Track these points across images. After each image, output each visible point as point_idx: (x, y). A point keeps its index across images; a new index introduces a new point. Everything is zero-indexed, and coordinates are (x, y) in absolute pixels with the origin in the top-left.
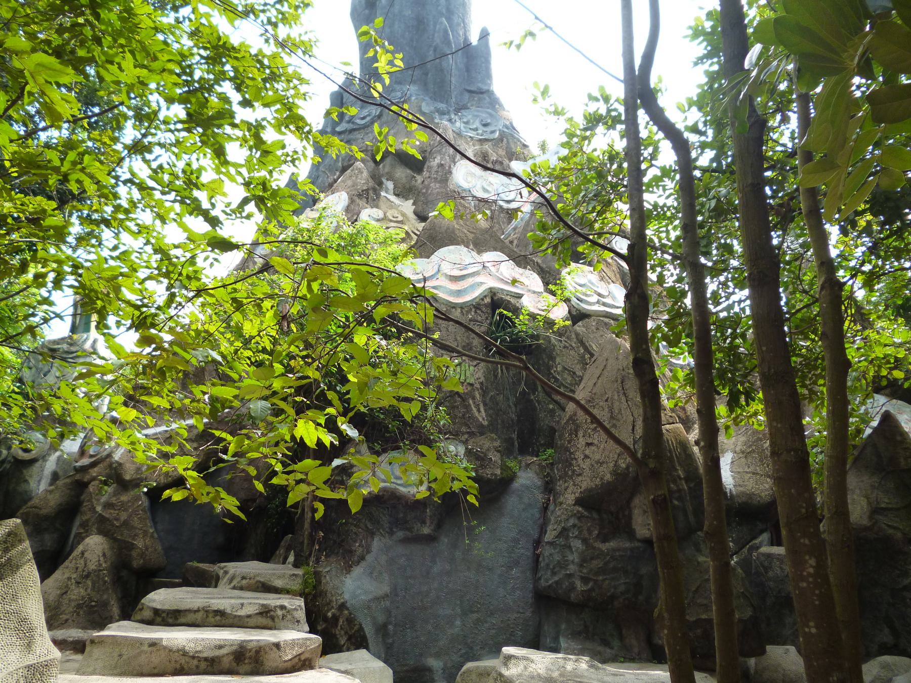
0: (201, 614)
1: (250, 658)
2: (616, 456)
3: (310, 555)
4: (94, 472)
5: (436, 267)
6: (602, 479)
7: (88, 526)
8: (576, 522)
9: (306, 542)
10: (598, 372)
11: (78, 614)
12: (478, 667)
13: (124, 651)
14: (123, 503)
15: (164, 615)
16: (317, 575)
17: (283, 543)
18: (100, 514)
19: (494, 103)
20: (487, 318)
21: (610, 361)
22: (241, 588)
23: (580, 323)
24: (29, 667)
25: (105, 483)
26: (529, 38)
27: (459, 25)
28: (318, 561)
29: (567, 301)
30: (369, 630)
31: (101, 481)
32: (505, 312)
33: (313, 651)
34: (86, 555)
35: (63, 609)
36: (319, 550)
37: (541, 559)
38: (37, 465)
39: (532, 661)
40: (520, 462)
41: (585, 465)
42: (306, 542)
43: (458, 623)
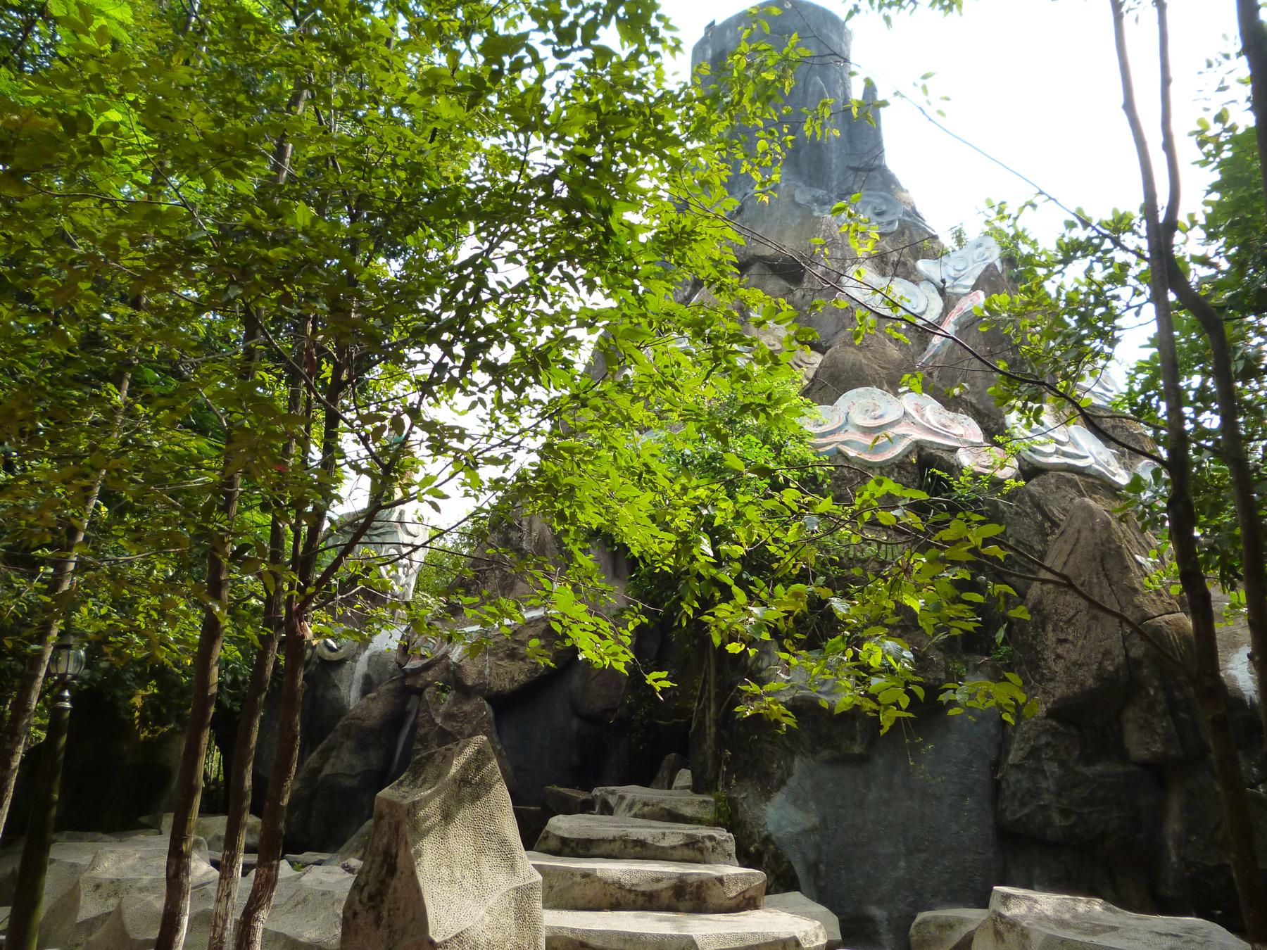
0: (618, 844)
1: (691, 893)
2: (1100, 656)
3: (717, 778)
4: (429, 676)
5: (843, 416)
6: (1082, 685)
8: (1050, 739)
9: (710, 762)
10: (1068, 548)
12: (936, 917)
13: (554, 882)
14: (466, 714)
15: (573, 845)
16: (732, 802)
17: (664, 764)
19: (888, 182)
20: (914, 481)
21: (1085, 533)
22: (644, 817)
23: (1034, 481)
24: (517, 889)
25: (443, 689)
26: (1028, 207)
27: (836, 81)
28: (727, 785)
29: (1017, 454)
30: (799, 869)
31: (438, 686)
32: (939, 472)
33: (757, 888)
36: (728, 772)
37: (1004, 785)
39: (1036, 902)
40: (966, 663)
41: (1058, 668)
42: (710, 762)
43: (902, 864)
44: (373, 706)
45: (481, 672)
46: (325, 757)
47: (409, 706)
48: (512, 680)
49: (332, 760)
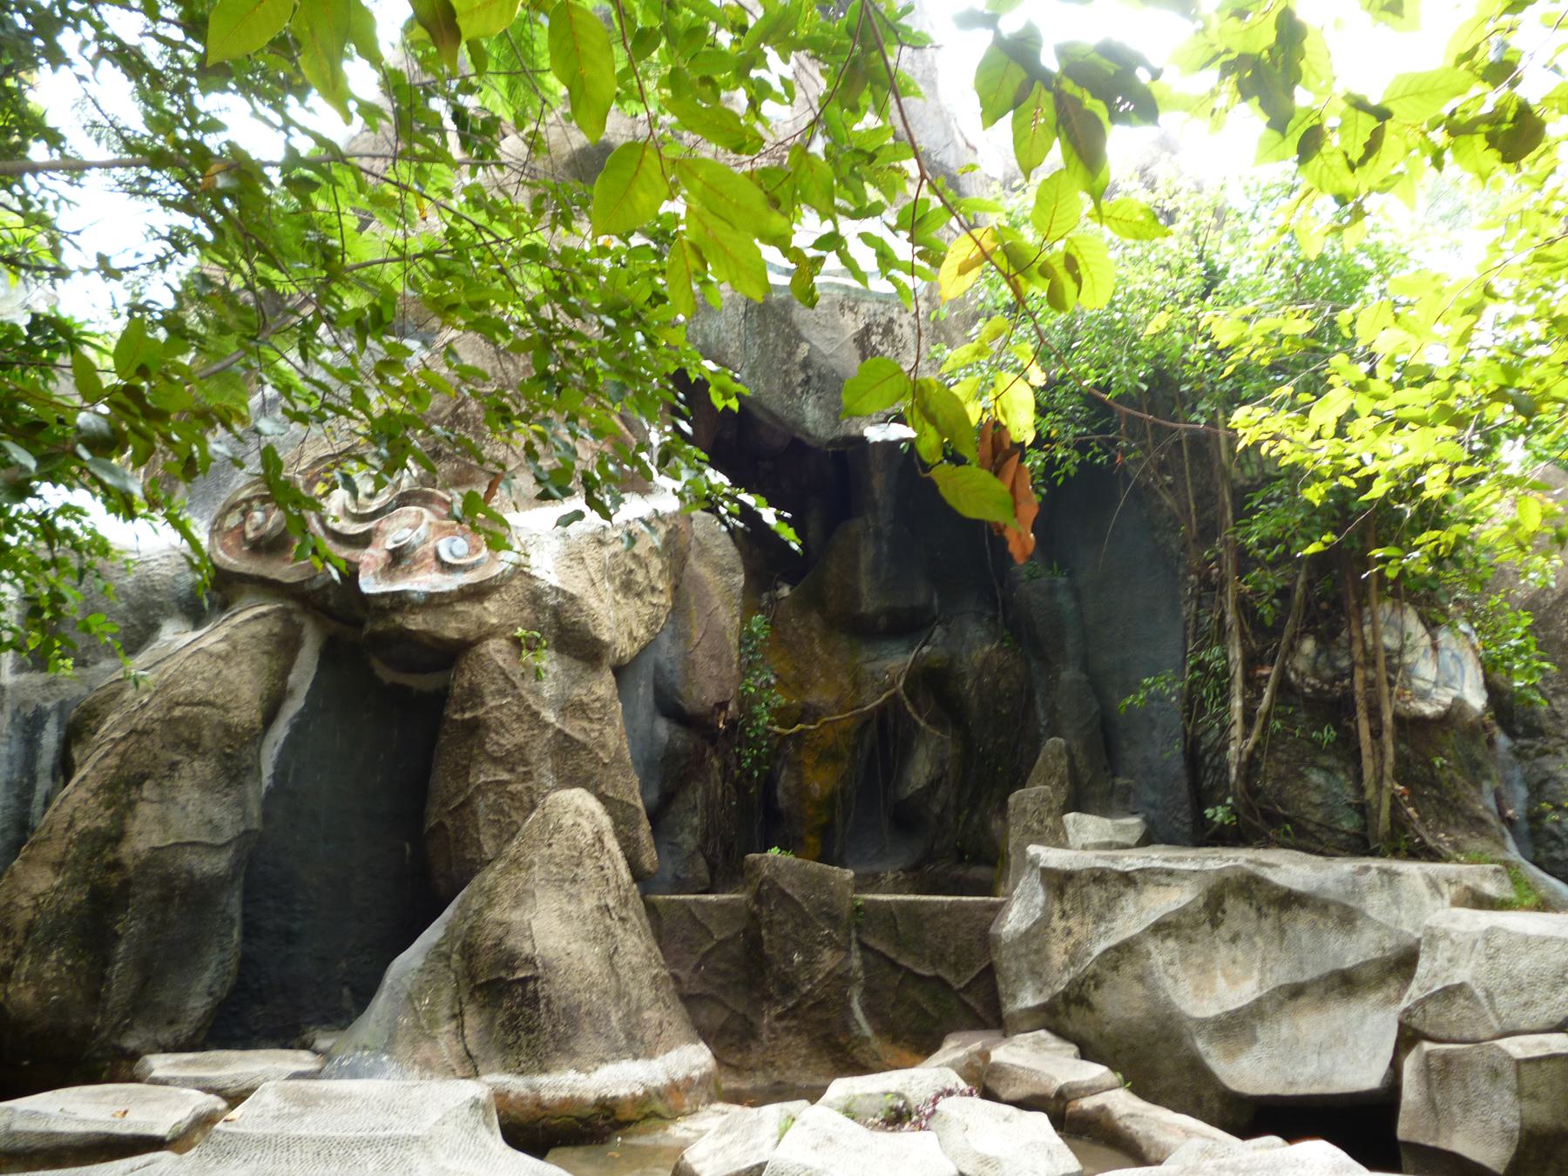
4: (492, 611)
7: (526, 763)
18: (559, 731)
35: (635, 993)
47: (292, 678)
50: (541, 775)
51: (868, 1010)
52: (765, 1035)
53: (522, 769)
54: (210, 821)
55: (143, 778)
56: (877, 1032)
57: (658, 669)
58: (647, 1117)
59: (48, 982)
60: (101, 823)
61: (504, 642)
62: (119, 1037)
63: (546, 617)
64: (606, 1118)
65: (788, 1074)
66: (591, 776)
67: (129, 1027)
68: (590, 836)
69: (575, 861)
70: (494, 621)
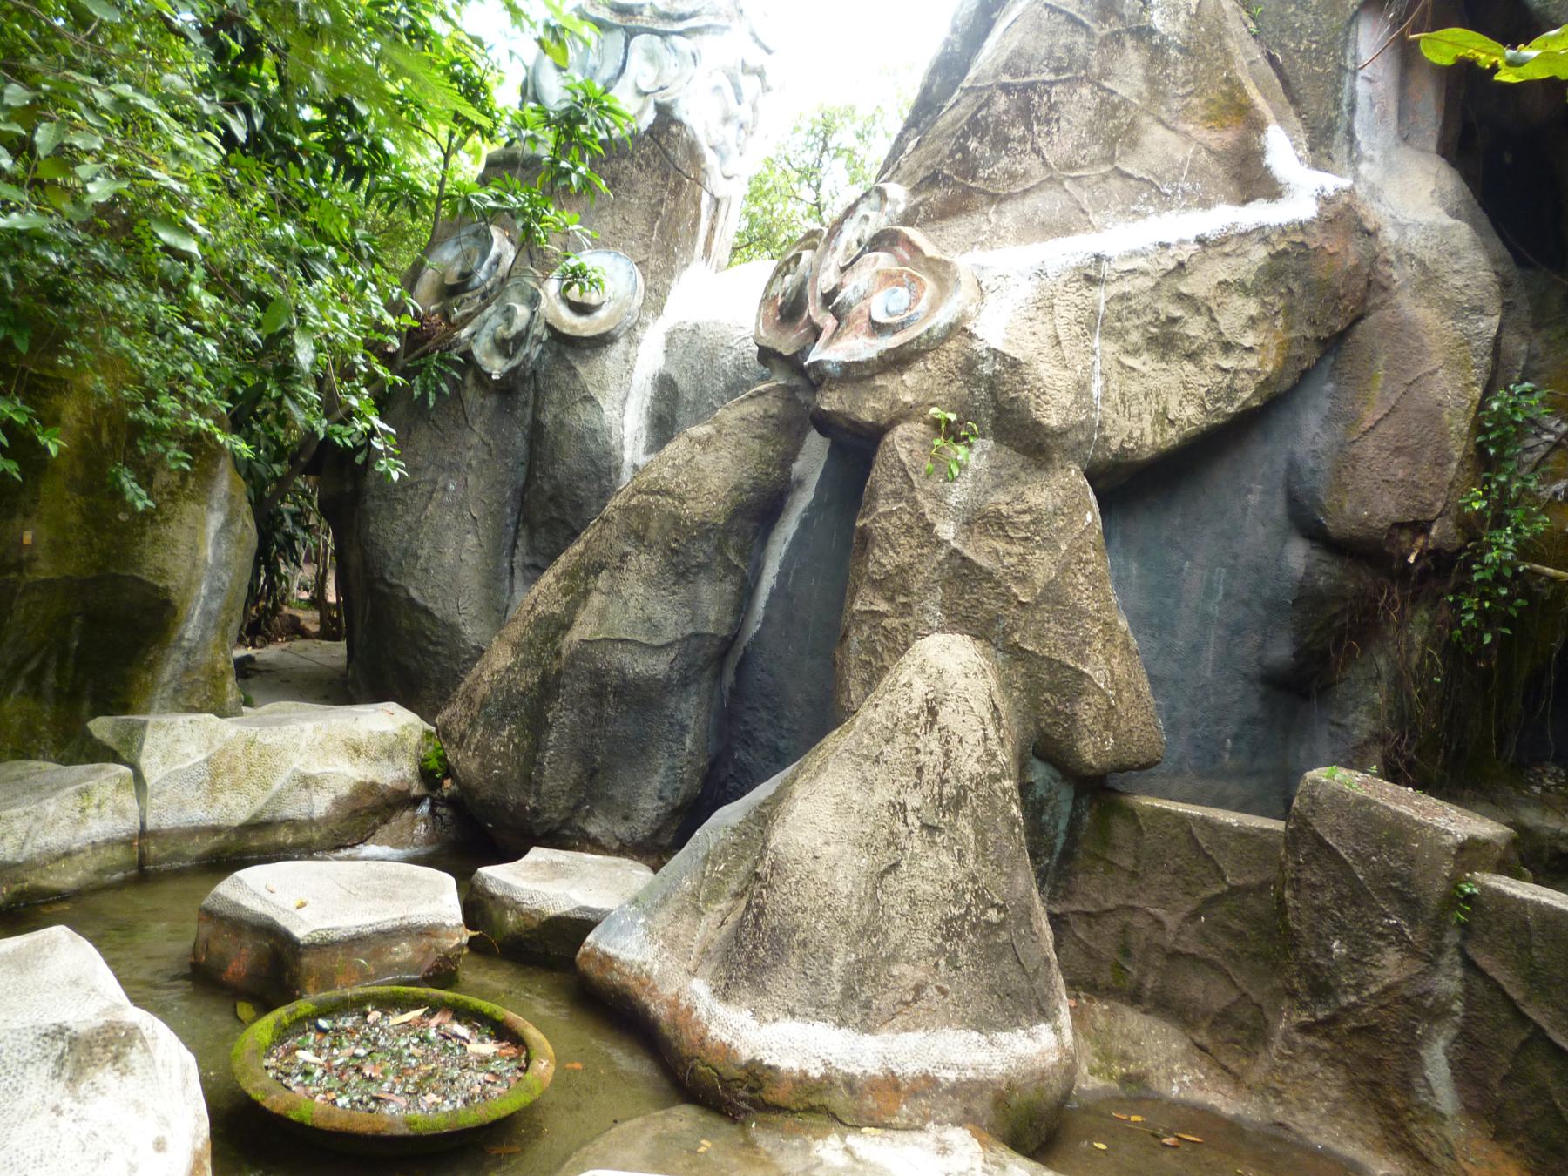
4: (907, 387)
7: (907, 591)
11: (952, 962)
18: (955, 553)
25: (952, 433)
34: (945, 715)
35: (896, 935)
38: (617, 351)
44: (704, 460)
45: (1082, 388)
46: (577, 593)
47: (797, 467)
48: (1162, 418)
49: (596, 600)
50: (924, 611)
51: (1465, 1072)
52: (1277, 1044)
53: (902, 599)
54: (649, 619)
55: (602, 567)
56: (1469, 1111)
57: (1293, 466)
58: (811, 1110)
59: (494, 755)
60: (557, 609)
61: (921, 426)
62: (584, 820)
63: (981, 392)
64: (752, 1090)
65: (1300, 1117)
66: (994, 620)
67: (590, 813)
68: (917, 702)
69: (887, 733)
70: (908, 398)
